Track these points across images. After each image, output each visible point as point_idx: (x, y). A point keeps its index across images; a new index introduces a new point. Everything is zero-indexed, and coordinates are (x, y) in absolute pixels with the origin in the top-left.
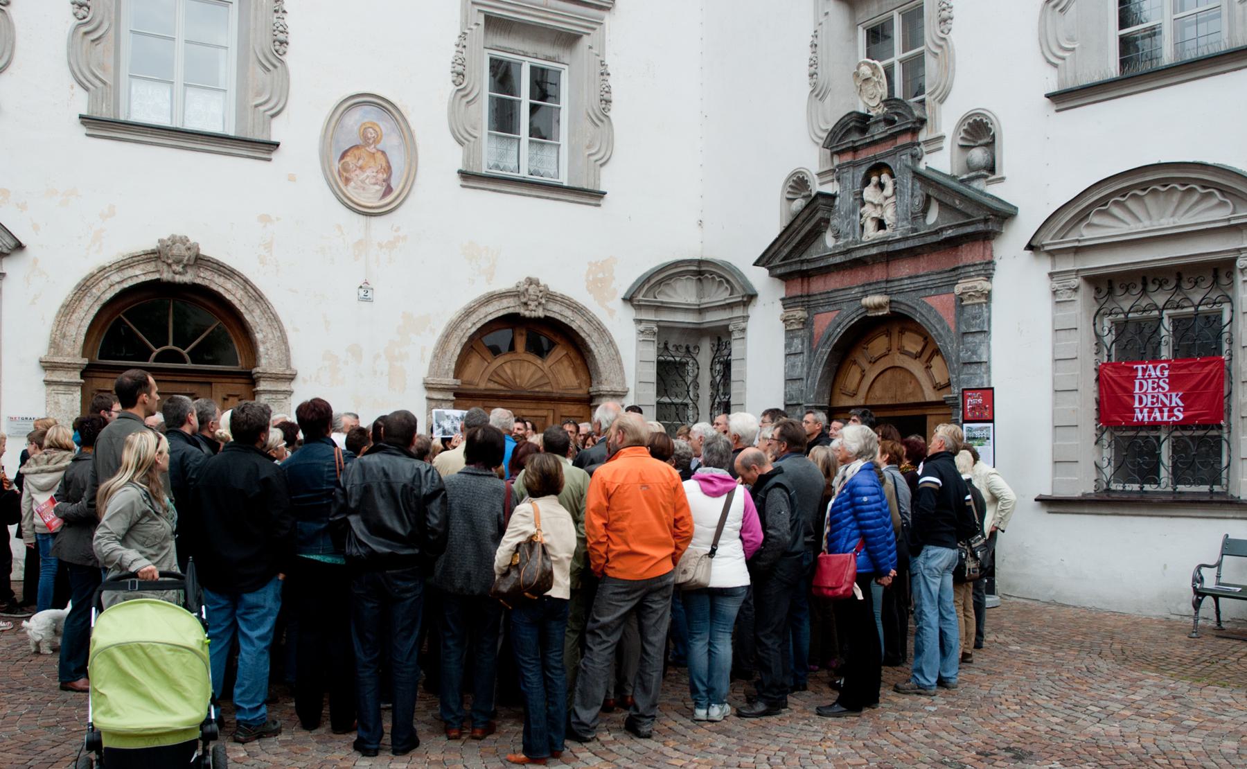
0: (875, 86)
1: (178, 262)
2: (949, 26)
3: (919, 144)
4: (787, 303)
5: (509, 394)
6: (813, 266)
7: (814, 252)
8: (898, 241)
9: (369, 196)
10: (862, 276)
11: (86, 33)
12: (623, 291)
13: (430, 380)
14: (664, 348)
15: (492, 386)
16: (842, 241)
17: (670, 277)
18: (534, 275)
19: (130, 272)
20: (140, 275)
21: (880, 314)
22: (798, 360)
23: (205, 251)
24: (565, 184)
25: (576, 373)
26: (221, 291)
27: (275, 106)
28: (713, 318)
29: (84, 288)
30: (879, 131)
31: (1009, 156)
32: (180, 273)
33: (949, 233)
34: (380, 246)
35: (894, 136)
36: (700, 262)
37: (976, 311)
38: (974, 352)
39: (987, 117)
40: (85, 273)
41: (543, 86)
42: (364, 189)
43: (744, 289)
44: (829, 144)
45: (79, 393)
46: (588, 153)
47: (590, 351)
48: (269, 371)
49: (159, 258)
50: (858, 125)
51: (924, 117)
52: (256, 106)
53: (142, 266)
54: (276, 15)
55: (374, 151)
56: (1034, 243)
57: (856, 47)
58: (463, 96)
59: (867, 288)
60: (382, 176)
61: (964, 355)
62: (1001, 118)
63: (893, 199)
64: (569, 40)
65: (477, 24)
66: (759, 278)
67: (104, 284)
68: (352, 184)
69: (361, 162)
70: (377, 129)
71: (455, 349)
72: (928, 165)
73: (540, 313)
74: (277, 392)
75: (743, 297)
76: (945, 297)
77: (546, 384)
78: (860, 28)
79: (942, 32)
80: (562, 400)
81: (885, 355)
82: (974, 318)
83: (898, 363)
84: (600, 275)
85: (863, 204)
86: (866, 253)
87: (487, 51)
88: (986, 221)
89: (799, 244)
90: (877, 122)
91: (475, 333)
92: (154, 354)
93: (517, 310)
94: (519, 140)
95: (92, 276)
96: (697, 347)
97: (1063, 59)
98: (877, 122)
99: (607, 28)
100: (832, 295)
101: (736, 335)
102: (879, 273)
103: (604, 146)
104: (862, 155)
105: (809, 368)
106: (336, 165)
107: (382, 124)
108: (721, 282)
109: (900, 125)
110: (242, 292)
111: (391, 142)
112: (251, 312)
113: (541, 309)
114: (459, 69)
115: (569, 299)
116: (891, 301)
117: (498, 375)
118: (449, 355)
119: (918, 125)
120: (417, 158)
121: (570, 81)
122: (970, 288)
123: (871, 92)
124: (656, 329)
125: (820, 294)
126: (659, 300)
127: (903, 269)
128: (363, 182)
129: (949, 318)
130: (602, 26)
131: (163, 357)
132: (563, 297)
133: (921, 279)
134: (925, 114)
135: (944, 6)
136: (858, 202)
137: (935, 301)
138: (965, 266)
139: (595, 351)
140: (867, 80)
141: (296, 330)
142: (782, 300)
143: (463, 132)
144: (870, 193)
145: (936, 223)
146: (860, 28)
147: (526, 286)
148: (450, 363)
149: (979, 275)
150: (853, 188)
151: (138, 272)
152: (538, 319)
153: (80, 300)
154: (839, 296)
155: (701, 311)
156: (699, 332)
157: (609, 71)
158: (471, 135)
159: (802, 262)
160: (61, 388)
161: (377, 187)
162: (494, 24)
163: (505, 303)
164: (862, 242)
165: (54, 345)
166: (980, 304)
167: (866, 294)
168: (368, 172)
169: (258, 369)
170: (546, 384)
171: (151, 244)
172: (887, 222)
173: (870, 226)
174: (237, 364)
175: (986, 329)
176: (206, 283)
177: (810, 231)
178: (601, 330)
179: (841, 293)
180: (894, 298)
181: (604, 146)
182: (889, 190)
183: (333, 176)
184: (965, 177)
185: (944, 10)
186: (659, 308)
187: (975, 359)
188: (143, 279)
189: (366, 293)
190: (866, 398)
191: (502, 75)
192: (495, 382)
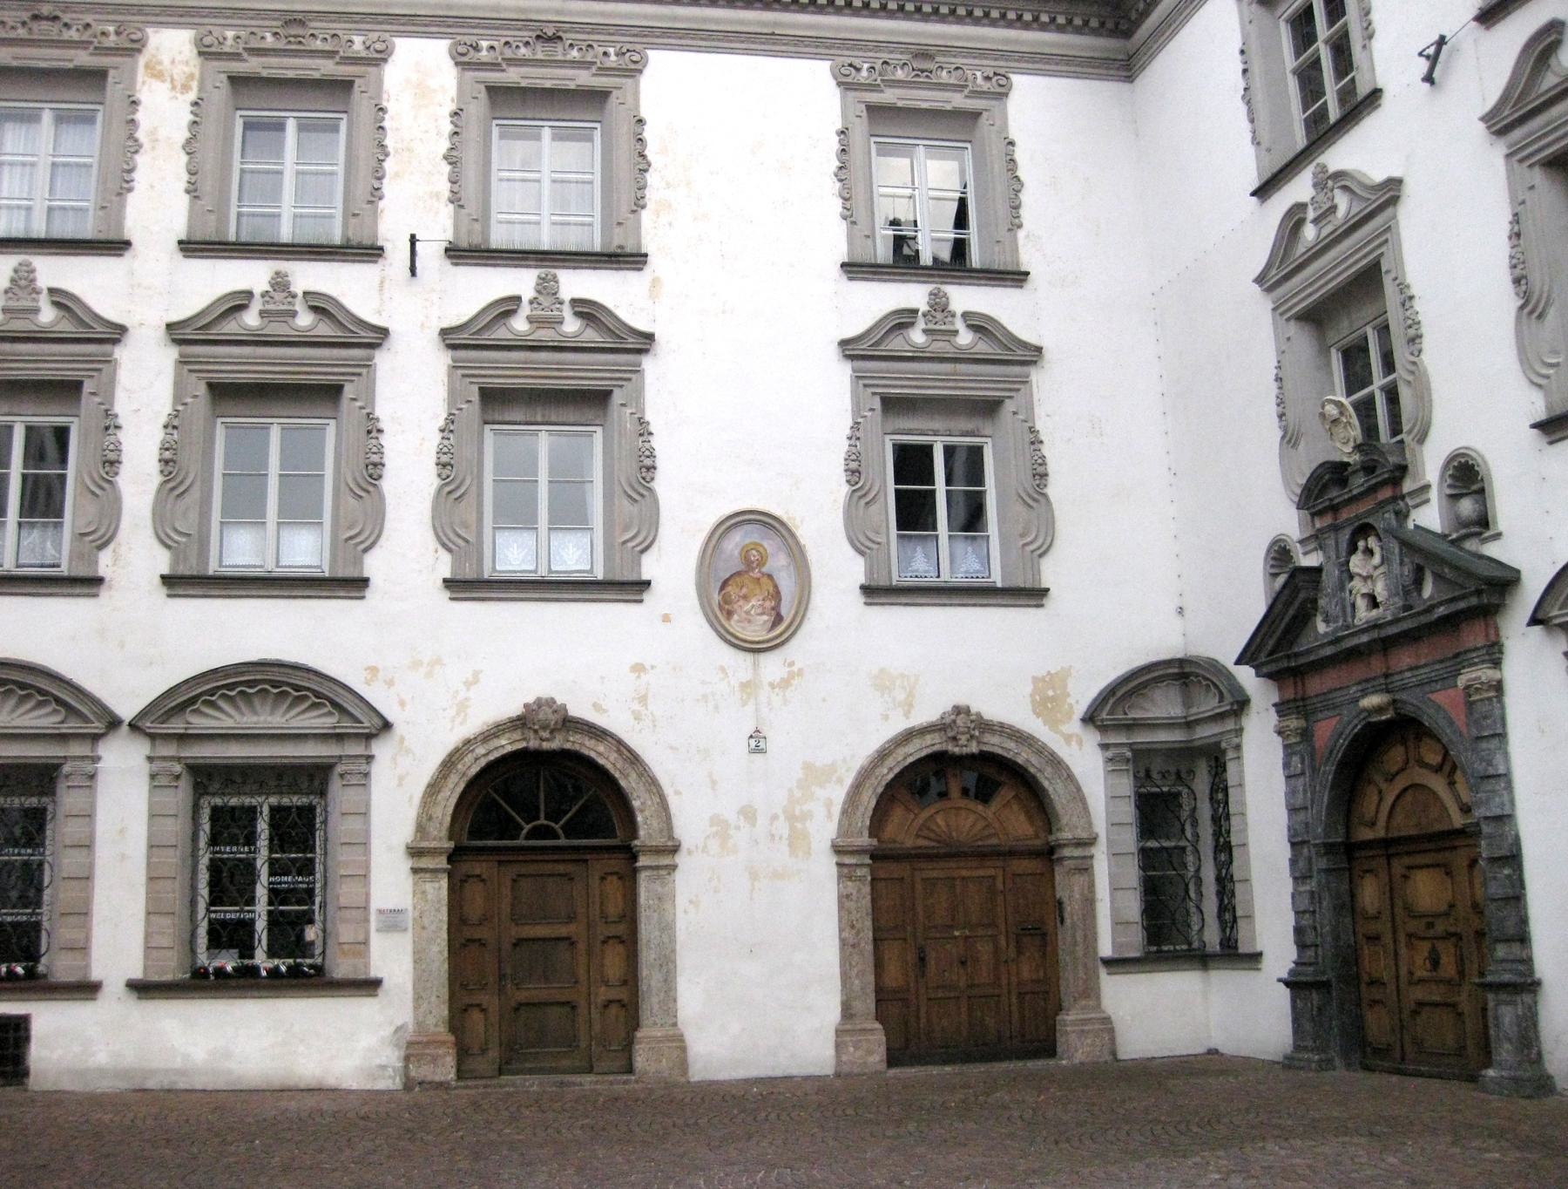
0: (1345, 427)
1: (544, 728)
2: (1417, 346)
3: (1403, 497)
4: (1282, 709)
5: (942, 851)
6: (1302, 661)
7: (1304, 644)
8: (1391, 623)
9: (756, 630)
10: (1359, 671)
11: (450, 493)
12: (1081, 708)
13: (840, 842)
14: (1143, 777)
15: (921, 842)
16: (1333, 626)
17: (1145, 685)
18: (962, 701)
19: (496, 743)
20: (506, 745)
21: (1384, 718)
22: (1300, 782)
23: (574, 711)
24: (999, 585)
25: (1030, 818)
26: (593, 755)
27: (645, 539)
28: (1205, 733)
29: (449, 764)
30: (1358, 483)
31: (1507, 506)
32: (547, 740)
33: (1441, 611)
34: (772, 686)
35: (1373, 489)
36: (1181, 662)
37: (1485, 708)
38: (1490, 763)
39: (1473, 459)
40: (450, 747)
41: (969, 464)
42: (749, 621)
43: (1232, 695)
44: (1305, 503)
45: (446, 880)
46: (1021, 543)
47: (1044, 790)
48: (648, 843)
49: (524, 725)
50: (1336, 476)
51: (1403, 463)
52: (624, 543)
53: (507, 735)
54: (641, 439)
55: (759, 575)
56: (1540, 616)
57: (1331, 374)
58: (860, 497)
59: (1364, 685)
60: (769, 604)
61: (1480, 767)
62: (1489, 458)
63: (1382, 570)
64: (989, 408)
65: (872, 410)
66: (1246, 676)
67: (469, 758)
68: (736, 617)
69: (744, 590)
70: (761, 549)
71: (869, 800)
72: (1417, 523)
73: (974, 748)
74: (658, 868)
75: (1232, 704)
76: (1451, 692)
77: (989, 836)
78: (1333, 351)
79: (1412, 354)
80: (1012, 853)
81: (1403, 769)
82: (1485, 718)
83: (1418, 780)
84: (1050, 693)
85: (1351, 577)
86: (1355, 641)
87: (888, 438)
88: (1479, 592)
89: (1287, 631)
90: (1355, 472)
91: (893, 780)
92: (524, 832)
93: (943, 747)
94: (937, 536)
95: (457, 750)
96: (1191, 772)
97: (1547, 377)
98: (1355, 472)
99: (1034, 387)
100: (1331, 696)
101: (1230, 754)
102: (1376, 665)
103: (1043, 531)
104: (1345, 514)
105: (1313, 793)
106: (716, 598)
107: (765, 544)
108: (1208, 686)
109: (1382, 474)
110: (616, 755)
111: (778, 563)
112: (626, 777)
113: (974, 744)
114: (854, 465)
115: (1010, 727)
116: (1394, 701)
117: (928, 829)
118: (862, 809)
119: (1397, 474)
120: (809, 576)
121: (994, 454)
122: (1475, 679)
123: (1342, 435)
124: (1129, 754)
125: (1316, 696)
126: (1130, 716)
127: (1403, 659)
128: (748, 613)
129: (1460, 719)
130: (1028, 386)
131: (536, 833)
132: (1002, 725)
133: (1422, 671)
134: (1405, 459)
135: (1410, 322)
136: (1345, 575)
137: (1440, 698)
138: (1466, 652)
139: (1050, 790)
140: (1335, 421)
141: (678, 793)
142: (1275, 705)
143: (863, 539)
144: (1357, 563)
145: (1431, 598)
146: (1333, 351)
147: (953, 717)
148: (863, 818)
149: (1483, 662)
150: (1338, 557)
151: (503, 742)
152: (972, 756)
153: (445, 777)
154: (1338, 697)
155: (1189, 725)
156: (1187, 754)
157: (1043, 438)
158: (873, 542)
159: (1288, 657)
160: (428, 875)
161: (765, 618)
162: (893, 405)
163: (928, 740)
164: (1355, 626)
165: (421, 829)
166: (1489, 699)
167: (1365, 693)
168: (754, 602)
169: (636, 842)
170: (989, 836)
171: (514, 709)
172: (1379, 599)
173: (1361, 604)
174: (616, 837)
175: (1499, 731)
176: (577, 747)
177: (1295, 617)
178: (1056, 762)
179: (1338, 694)
180: (1397, 697)
181: (1043, 531)
182: (1377, 559)
183: (713, 611)
184: (1454, 536)
185: (1410, 327)
186: (1132, 726)
187: (1491, 771)
188: (509, 749)
189: (757, 743)
190: (1387, 828)
191: (912, 463)
192: (925, 838)
